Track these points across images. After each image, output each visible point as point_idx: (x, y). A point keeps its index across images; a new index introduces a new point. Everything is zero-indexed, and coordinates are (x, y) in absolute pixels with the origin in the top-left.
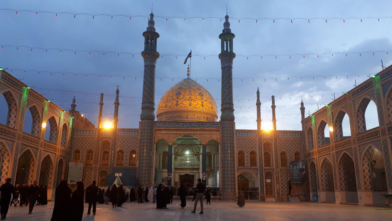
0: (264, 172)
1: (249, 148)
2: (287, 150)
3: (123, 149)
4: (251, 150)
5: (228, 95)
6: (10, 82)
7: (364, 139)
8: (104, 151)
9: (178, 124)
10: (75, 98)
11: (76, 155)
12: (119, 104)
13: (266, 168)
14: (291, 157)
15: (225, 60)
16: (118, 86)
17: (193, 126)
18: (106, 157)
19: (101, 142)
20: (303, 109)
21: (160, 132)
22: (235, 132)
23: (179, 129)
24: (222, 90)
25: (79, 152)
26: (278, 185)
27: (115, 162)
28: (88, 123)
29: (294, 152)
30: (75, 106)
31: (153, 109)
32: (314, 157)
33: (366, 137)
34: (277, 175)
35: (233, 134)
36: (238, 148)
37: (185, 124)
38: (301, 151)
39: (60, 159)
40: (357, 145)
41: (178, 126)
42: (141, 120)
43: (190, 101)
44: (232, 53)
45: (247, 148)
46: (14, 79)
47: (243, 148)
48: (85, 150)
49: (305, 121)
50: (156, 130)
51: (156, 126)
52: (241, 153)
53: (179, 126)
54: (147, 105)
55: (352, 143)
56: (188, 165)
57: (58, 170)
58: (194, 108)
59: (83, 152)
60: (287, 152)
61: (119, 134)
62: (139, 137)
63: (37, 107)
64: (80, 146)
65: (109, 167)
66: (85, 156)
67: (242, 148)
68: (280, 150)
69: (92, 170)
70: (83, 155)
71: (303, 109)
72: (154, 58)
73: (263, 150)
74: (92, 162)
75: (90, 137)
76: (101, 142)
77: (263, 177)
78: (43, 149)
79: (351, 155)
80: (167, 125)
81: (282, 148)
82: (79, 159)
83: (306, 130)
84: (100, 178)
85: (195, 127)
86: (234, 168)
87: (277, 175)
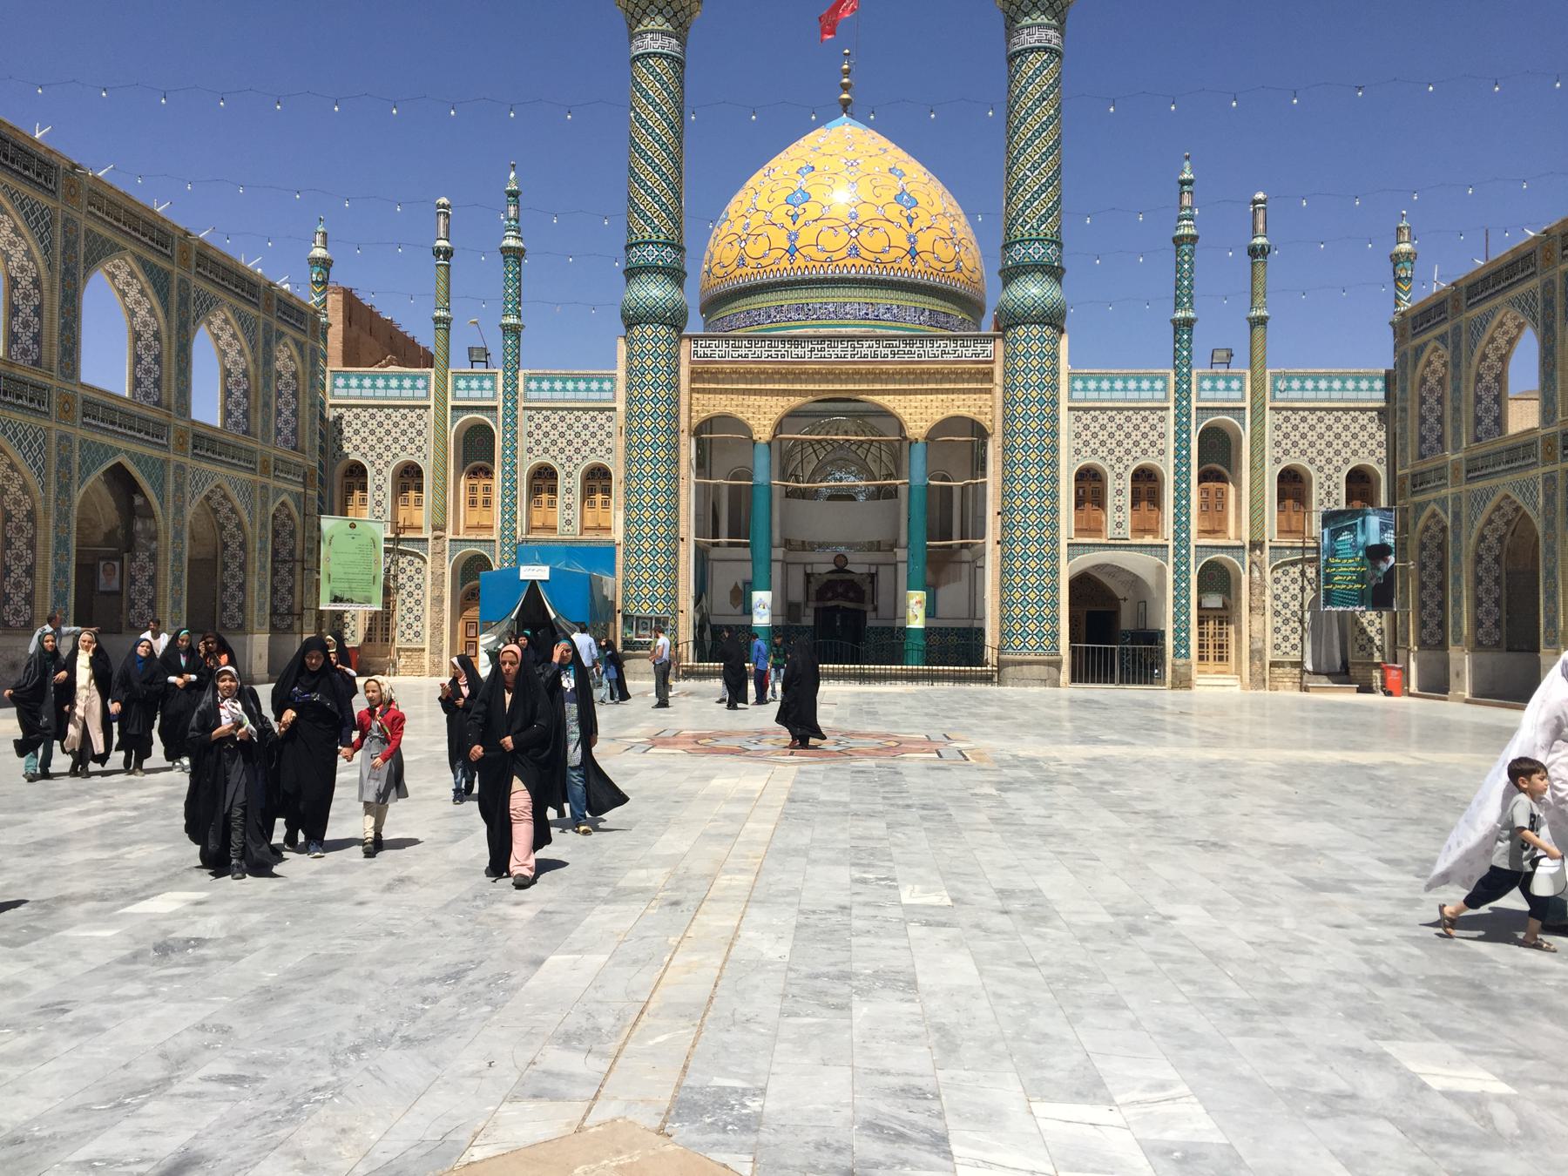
1: (1128, 452)
2: (1312, 461)
3: (552, 462)
4: (1100, 463)
14: (1329, 494)
18: (480, 496)
36: (1078, 452)
43: (854, 234)
45: (1120, 452)
47: (554, 450)
48: (1338, 469)
60: (1312, 469)
62: (621, 406)
77: (1188, 586)
80: (743, 351)
85: (876, 356)
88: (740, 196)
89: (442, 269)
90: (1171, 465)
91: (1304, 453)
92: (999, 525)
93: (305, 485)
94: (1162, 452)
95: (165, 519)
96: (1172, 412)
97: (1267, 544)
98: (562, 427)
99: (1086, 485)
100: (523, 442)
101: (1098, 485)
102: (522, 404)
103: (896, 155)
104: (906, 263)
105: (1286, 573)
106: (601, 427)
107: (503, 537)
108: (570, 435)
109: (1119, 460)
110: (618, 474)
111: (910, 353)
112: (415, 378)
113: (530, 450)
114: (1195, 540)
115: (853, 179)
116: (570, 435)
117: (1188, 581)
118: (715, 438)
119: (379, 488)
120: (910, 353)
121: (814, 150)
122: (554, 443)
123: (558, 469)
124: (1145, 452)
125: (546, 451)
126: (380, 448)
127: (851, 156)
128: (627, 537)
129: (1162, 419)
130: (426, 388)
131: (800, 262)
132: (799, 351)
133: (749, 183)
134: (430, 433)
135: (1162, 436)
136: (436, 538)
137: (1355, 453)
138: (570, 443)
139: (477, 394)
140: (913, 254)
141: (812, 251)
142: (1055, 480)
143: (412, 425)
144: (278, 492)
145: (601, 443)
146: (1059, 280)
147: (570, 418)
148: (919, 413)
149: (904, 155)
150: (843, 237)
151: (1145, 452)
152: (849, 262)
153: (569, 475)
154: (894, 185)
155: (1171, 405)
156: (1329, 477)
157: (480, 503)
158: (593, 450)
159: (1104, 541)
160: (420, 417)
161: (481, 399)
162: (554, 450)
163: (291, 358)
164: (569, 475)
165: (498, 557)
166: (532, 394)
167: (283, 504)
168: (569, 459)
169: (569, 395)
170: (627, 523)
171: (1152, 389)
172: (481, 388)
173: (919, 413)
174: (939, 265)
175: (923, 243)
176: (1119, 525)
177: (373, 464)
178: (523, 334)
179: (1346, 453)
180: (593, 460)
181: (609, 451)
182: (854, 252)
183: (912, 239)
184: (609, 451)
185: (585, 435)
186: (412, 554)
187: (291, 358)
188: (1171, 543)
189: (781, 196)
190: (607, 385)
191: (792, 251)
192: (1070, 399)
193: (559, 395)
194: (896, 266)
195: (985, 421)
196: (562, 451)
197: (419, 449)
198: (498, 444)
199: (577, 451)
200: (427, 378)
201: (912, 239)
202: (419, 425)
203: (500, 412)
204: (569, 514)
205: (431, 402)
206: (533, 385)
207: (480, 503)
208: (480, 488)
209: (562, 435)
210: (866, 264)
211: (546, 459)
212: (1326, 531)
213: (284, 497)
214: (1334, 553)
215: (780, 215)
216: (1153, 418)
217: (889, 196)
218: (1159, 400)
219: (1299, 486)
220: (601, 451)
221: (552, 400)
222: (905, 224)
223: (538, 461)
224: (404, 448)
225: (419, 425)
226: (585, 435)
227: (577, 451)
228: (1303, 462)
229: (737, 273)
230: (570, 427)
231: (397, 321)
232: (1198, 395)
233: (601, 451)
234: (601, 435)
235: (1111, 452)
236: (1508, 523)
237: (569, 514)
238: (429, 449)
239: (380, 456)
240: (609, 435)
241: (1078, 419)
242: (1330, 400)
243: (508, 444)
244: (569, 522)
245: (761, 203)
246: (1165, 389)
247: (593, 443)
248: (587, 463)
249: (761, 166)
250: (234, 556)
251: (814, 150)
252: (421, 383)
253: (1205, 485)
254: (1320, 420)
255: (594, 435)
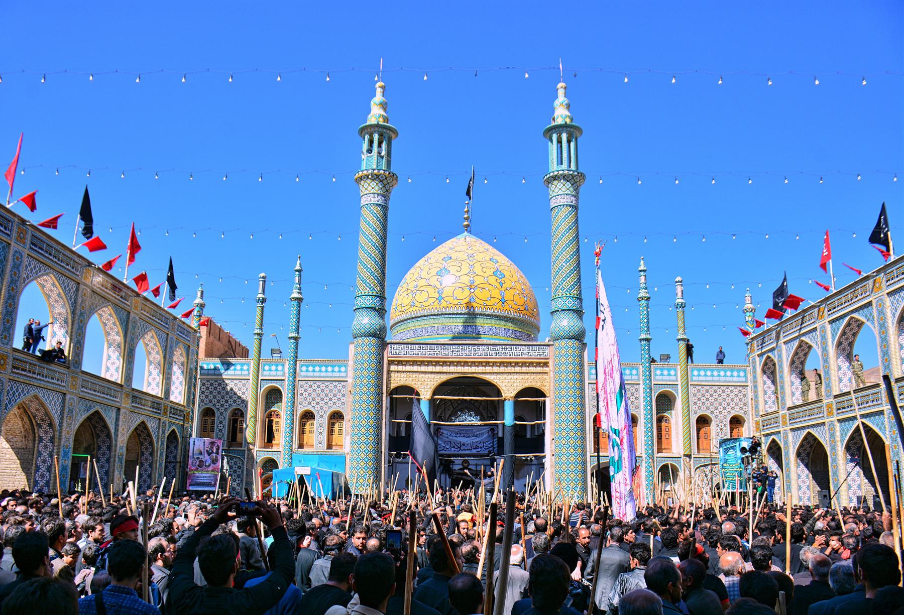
3: (312, 410)
6: (50, 254)
7: (844, 408)
11: (206, 422)
25: (213, 414)
28: (233, 344)
29: (729, 417)
32: (880, 409)
33: (808, 412)
46: (59, 248)
48: (226, 410)
50: (390, 363)
55: (825, 413)
56: (469, 447)
57: (167, 457)
62: (350, 380)
66: (226, 423)
68: (695, 412)
70: (221, 422)
78: (27, 252)
79: (880, 429)
80: (416, 352)
81: (699, 408)
82: (212, 430)
83: (894, 315)
88: (412, 270)
89: (295, 303)
90: (642, 414)
91: (708, 408)
92: (554, 447)
93: (183, 421)
94: (637, 407)
95: (157, 442)
98: (319, 391)
103: (493, 251)
106: (339, 391)
108: (322, 395)
111: (505, 353)
115: (471, 263)
116: (322, 395)
120: (505, 353)
121: (451, 249)
122: (314, 399)
125: (309, 403)
127: (470, 252)
128: (353, 451)
129: (637, 390)
132: (446, 352)
133: (418, 264)
135: (637, 399)
138: (322, 399)
139: (274, 373)
144: (171, 424)
146: (581, 318)
147: (323, 386)
148: (509, 386)
149: (497, 252)
154: (492, 267)
155: (641, 382)
158: (335, 403)
160: (244, 385)
162: (314, 403)
163: (181, 355)
164: (321, 416)
166: (304, 372)
167: (173, 431)
168: (322, 408)
173: (509, 386)
175: (509, 295)
177: (218, 409)
178: (300, 341)
180: (335, 408)
184: (343, 404)
185: (331, 395)
187: (181, 355)
189: (434, 272)
190: (343, 369)
191: (440, 299)
193: (318, 374)
196: (318, 403)
205: (251, 377)
206: (304, 369)
208: (209, 421)
209: (318, 395)
212: (721, 449)
213: (174, 427)
214: (726, 461)
215: (433, 281)
220: (339, 404)
222: (499, 286)
223: (305, 409)
224: (335, 403)
226: (331, 395)
229: (411, 310)
230: (323, 391)
231: (232, 333)
233: (339, 404)
234: (339, 395)
236: (811, 447)
239: (222, 406)
240: (343, 395)
242: (719, 381)
245: (424, 274)
246: (638, 374)
247: (335, 399)
249: (423, 256)
250: (147, 459)
251: (451, 249)
252: (245, 367)
254: (715, 391)
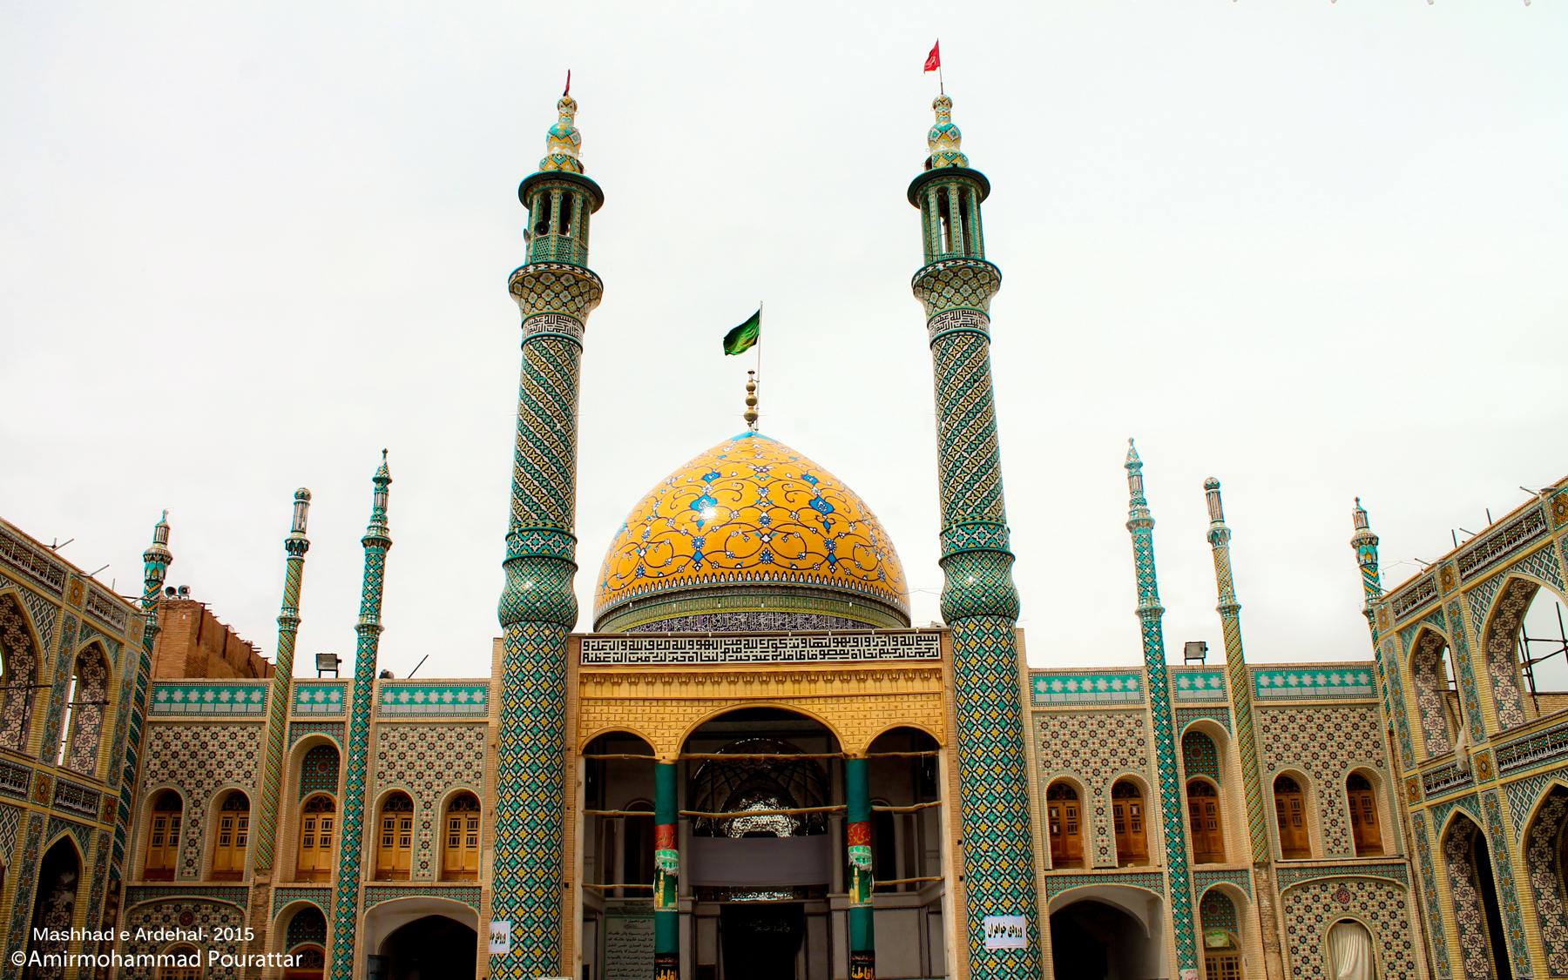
0: (1192, 890)
1: (1105, 762)
2: (1307, 766)
4: (1074, 776)
5: (975, 478)
8: (308, 795)
9: (708, 646)
10: (168, 518)
12: (386, 544)
13: (1200, 867)
14: (1331, 803)
15: (949, 300)
16: (385, 452)
17: (789, 651)
18: (319, 833)
19: (294, 746)
20: (1366, 544)
21: (606, 691)
22: (1024, 678)
23: (711, 674)
24: (943, 452)
26: (1272, 958)
27: (363, 860)
30: (166, 559)
31: (568, 566)
34: (1265, 903)
35: (1015, 689)
36: (1047, 764)
37: (747, 646)
38: (1379, 763)
39: (54, 841)
40: (49, 811)
41: (705, 653)
42: (504, 625)
43: (766, 539)
44: (982, 265)
45: (1095, 763)
47: (1076, 763)
48: (1336, 775)
49: (1381, 610)
50: (585, 679)
51: (586, 656)
52: (1062, 792)
53: (711, 653)
54: (536, 543)
58: (789, 572)
59: (197, 803)
60: (1309, 775)
61: (383, 702)
62: (494, 721)
63: (21, 599)
64: (182, 774)
65: (331, 885)
67: (1067, 763)
69: (244, 901)
71: (1366, 544)
72: (573, 299)
73: (1181, 771)
74: (246, 860)
75: (197, 723)
76: (294, 746)
77: (1191, 922)
80: (643, 654)
81: (1279, 757)
84: (366, 907)
85: (802, 657)
86: (1030, 875)
87: (1265, 903)
91: (1297, 757)
92: (961, 856)
94: (1143, 762)
96: (1149, 715)
97: (1274, 865)
99: (1059, 804)
100: (375, 765)
101: (1072, 804)
102: (374, 720)
104: (825, 570)
105: (1298, 900)
107: (341, 883)
109: (1096, 772)
110: (487, 801)
112: (250, 689)
113: (1047, 764)
114: (1193, 867)
117: (1190, 915)
118: (616, 757)
119: (427, 825)
122: (411, 766)
123: (415, 798)
124: (1124, 762)
125: (401, 776)
126: (430, 776)
130: (263, 701)
131: (840, 573)
134: (262, 756)
135: (1141, 742)
136: (258, 886)
137: (1351, 755)
140: (832, 560)
141: (721, 558)
142: (1024, 799)
143: (470, 746)
145: (469, 765)
150: (754, 543)
151: (1124, 762)
152: (762, 568)
153: (428, 805)
155: (1148, 705)
156: (1329, 784)
157: (234, 841)
158: (458, 774)
159: (1088, 871)
160: (252, 736)
161: (327, 713)
162: (410, 775)
165: (334, 910)
169: (431, 709)
170: (498, 864)
171: (1125, 689)
172: (327, 701)
174: (861, 573)
176: (1103, 850)
177: (190, 793)
179: (1342, 755)
181: (478, 775)
182: (767, 557)
183: (830, 545)
184: (478, 775)
186: (1390, 883)
188: (1165, 870)
192: (1034, 703)
194: (814, 573)
195: (936, 730)
197: (248, 775)
198: (344, 767)
199: (439, 775)
200: (264, 690)
201: (830, 545)
202: (251, 746)
203: (349, 729)
204: (425, 855)
205: (268, 718)
207: (234, 841)
210: (727, 572)
211: (401, 786)
216: (1130, 723)
217: (802, 500)
218: (1133, 702)
219: (1365, 793)
220: (468, 775)
221: (411, 714)
225: (251, 746)
227: (439, 775)
228: (1298, 767)
232: (1176, 695)
235: (1086, 763)
237: (425, 855)
238: (260, 775)
240: (479, 756)
241: (1044, 726)
243: (355, 767)
244: (424, 865)
248: (452, 789)
252: (256, 696)
253: (1195, 799)
255: (460, 756)
